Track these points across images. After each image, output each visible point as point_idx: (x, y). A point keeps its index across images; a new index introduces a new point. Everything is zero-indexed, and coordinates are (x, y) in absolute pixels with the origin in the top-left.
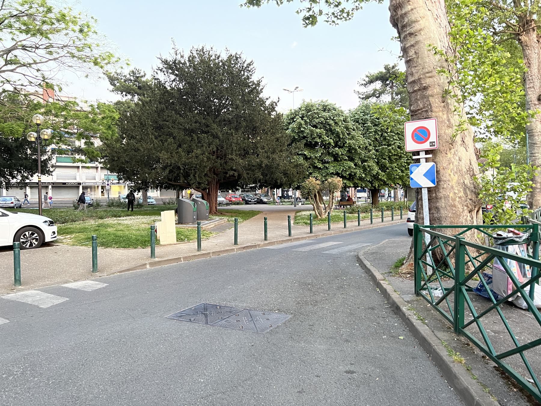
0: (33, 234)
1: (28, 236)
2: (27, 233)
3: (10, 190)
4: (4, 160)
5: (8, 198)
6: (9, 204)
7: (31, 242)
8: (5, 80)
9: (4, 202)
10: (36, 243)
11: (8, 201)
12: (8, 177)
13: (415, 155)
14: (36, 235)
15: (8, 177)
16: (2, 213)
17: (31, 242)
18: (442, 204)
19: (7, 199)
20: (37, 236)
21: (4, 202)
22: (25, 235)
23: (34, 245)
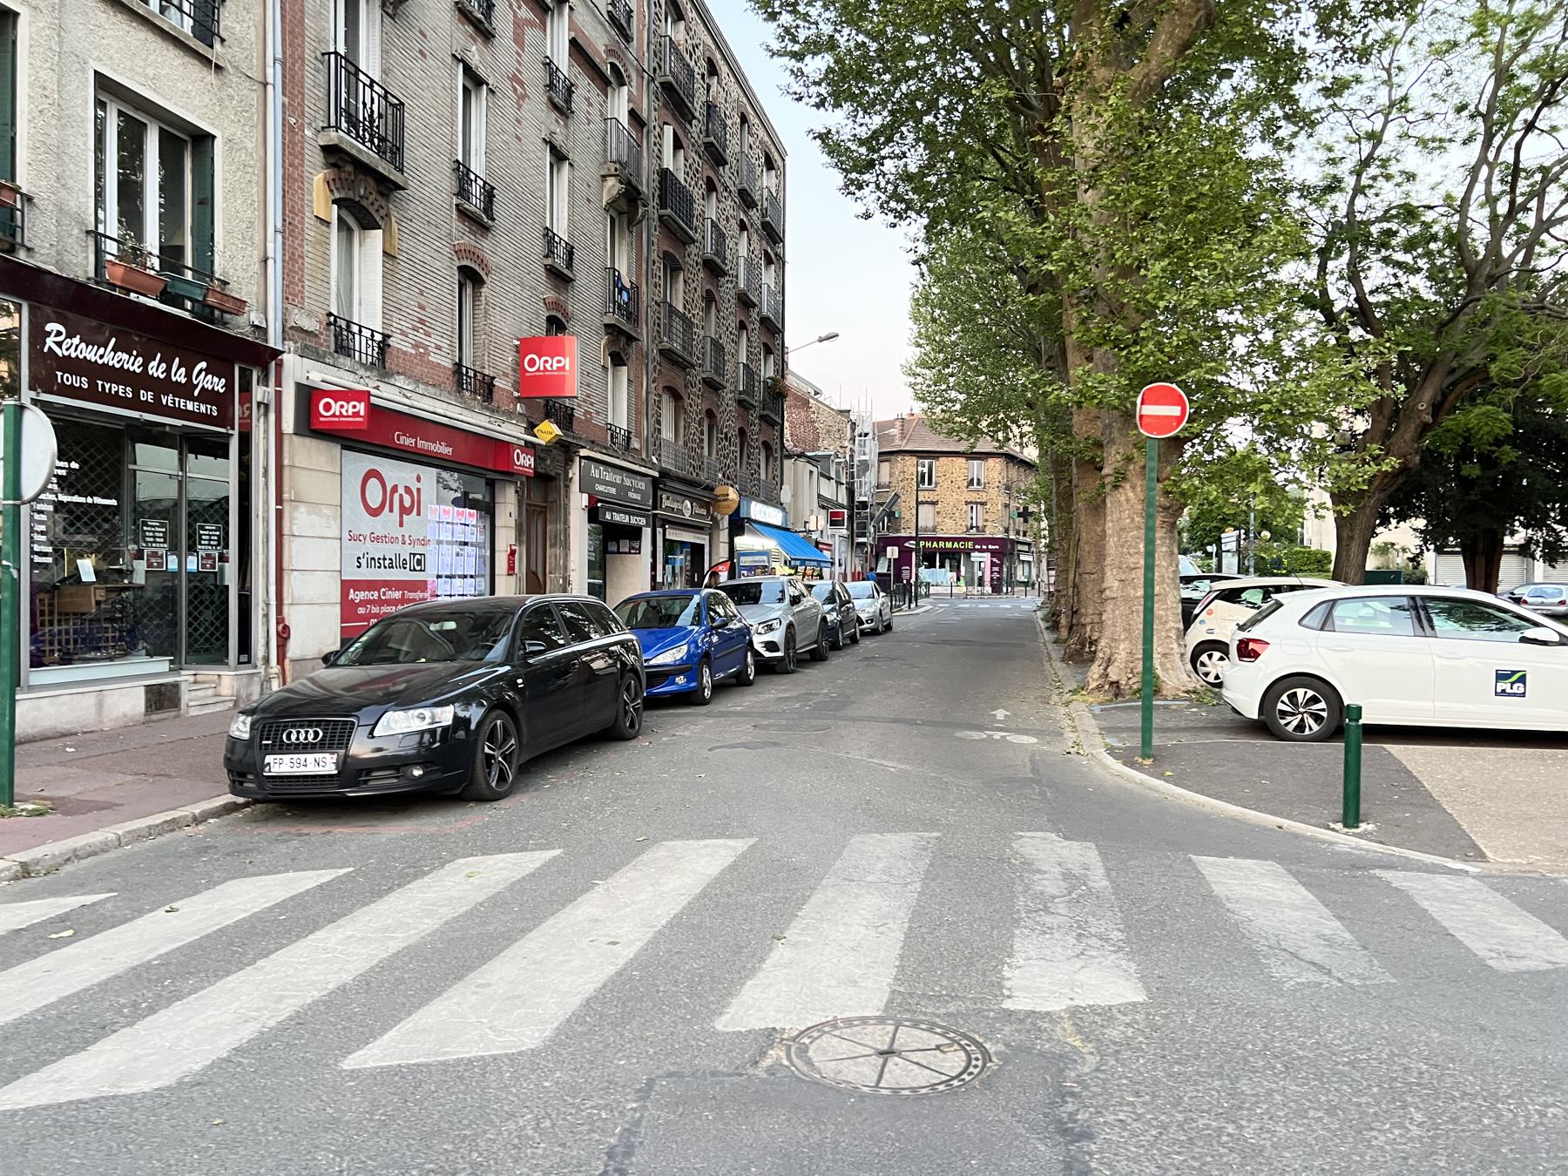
0: (1314, 700)
1: (1300, 701)
2: (1300, 692)
3: (1560, 565)
4: (1548, 477)
5: (1550, 589)
6: (1552, 604)
7: (1302, 720)
8: (1559, 244)
9: (1540, 600)
10: (1316, 728)
11: (1553, 596)
12: (1555, 526)
13: (47, 564)
14: (1322, 705)
15: (1555, 526)
16: (1560, 634)
17: (1302, 720)
18: (106, 707)
19: (1549, 591)
20: (1323, 710)
21: (1540, 600)
22: (1295, 694)
23: (1307, 732)
